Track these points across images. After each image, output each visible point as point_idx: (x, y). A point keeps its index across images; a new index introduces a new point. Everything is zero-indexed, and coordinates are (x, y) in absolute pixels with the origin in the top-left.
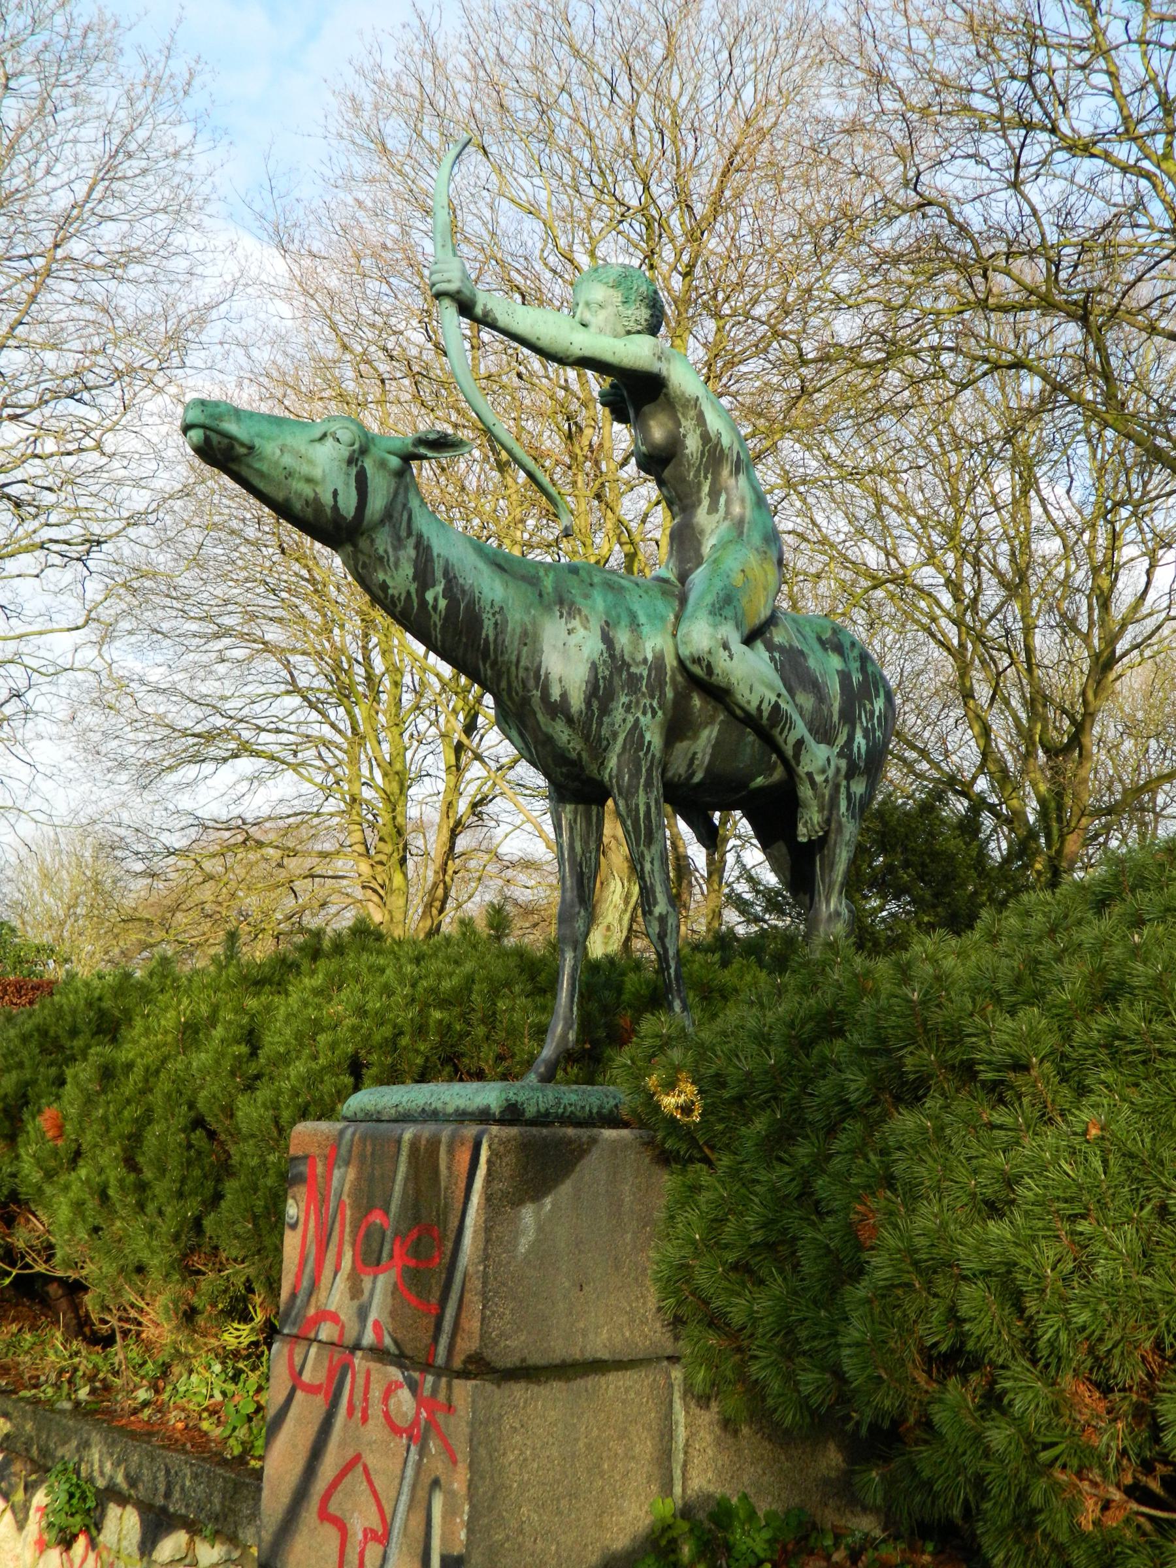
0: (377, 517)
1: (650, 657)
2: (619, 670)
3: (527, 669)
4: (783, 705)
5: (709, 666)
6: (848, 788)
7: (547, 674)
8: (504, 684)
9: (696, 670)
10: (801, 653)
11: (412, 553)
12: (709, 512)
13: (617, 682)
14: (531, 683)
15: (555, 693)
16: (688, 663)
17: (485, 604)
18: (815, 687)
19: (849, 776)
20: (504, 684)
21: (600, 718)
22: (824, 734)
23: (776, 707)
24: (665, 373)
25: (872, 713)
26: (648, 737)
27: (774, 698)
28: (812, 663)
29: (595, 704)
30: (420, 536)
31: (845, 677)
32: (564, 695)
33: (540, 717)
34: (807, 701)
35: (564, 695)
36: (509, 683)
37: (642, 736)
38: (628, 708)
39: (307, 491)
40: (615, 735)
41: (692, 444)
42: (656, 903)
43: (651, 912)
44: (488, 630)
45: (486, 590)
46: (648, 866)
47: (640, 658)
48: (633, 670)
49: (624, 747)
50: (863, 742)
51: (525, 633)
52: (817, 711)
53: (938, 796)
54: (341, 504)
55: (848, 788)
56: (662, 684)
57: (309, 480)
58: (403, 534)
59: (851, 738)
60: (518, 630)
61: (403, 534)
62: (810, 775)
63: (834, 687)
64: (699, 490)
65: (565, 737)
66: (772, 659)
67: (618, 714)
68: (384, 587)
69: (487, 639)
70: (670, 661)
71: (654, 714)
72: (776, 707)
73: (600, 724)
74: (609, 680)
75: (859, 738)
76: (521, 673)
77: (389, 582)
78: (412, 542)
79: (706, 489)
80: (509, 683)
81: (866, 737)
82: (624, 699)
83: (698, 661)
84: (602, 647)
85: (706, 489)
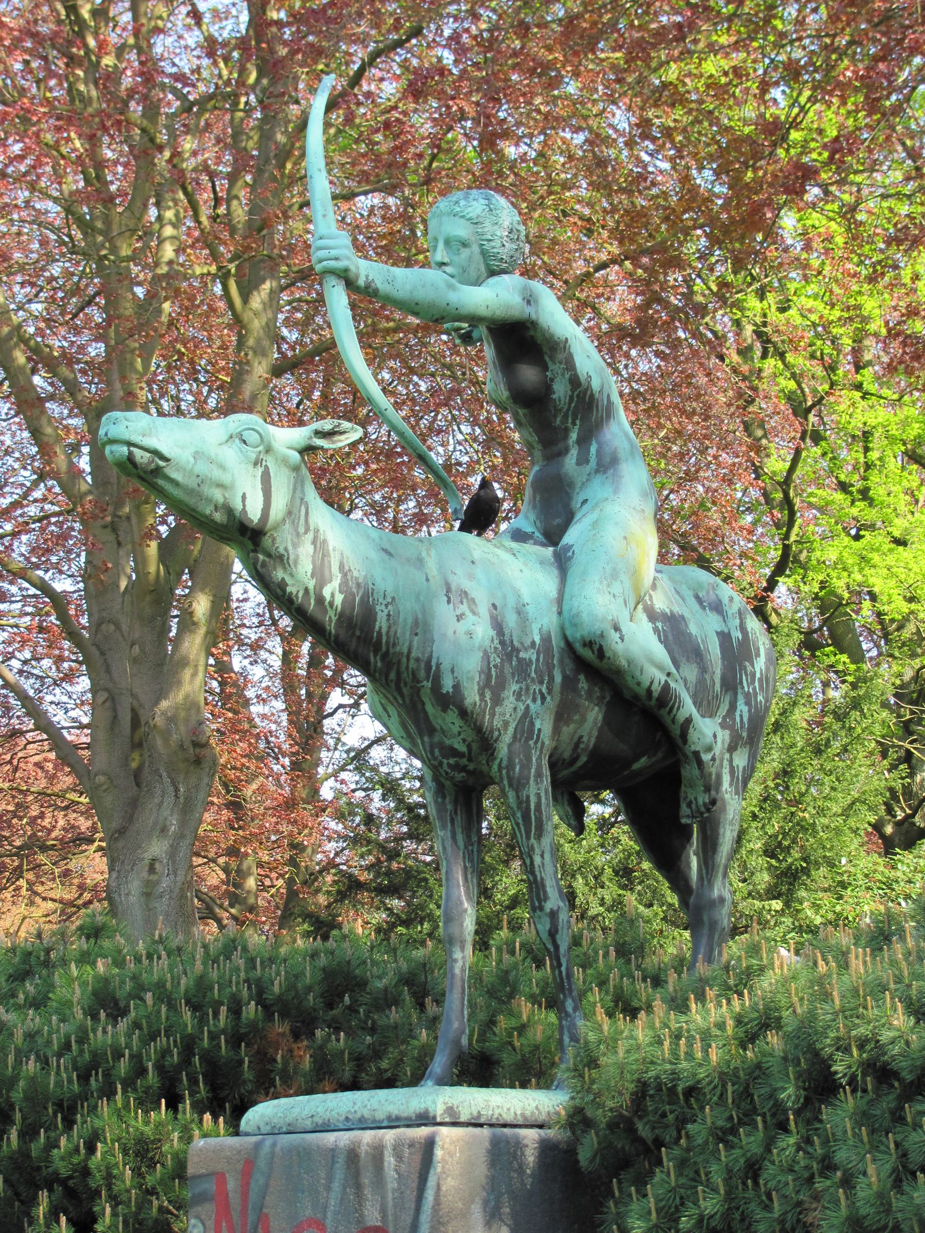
0: (280, 516)
1: (537, 639)
2: (509, 656)
3: (418, 660)
4: (673, 685)
5: (601, 649)
6: (731, 761)
7: (438, 665)
8: (393, 676)
9: (587, 654)
10: (682, 617)
11: (311, 549)
12: (579, 463)
13: (507, 670)
14: (422, 674)
15: (447, 685)
16: (578, 647)
17: (379, 596)
18: (696, 654)
19: (731, 749)
20: (393, 676)
21: (493, 709)
22: (707, 706)
23: (666, 686)
24: (534, 317)
25: (753, 675)
26: (538, 725)
27: (663, 678)
28: (693, 629)
29: (488, 695)
30: (317, 531)
31: (724, 637)
32: (457, 687)
33: (429, 708)
34: (691, 672)
35: (457, 687)
36: (399, 674)
37: (532, 724)
38: (518, 696)
39: (218, 496)
40: (506, 724)
41: (560, 390)
42: (546, 898)
43: (541, 908)
44: (381, 622)
45: (379, 582)
46: (537, 860)
47: (528, 643)
48: (522, 655)
49: (515, 737)
50: (745, 709)
51: (416, 623)
52: (701, 682)
53: (882, 836)
54: (248, 508)
55: (731, 761)
56: (550, 668)
57: (220, 485)
58: (302, 530)
59: (733, 707)
60: (410, 621)
61: (302, 530)
62: (697, 754)
63: (714, 650)
64: (566, 437)
65: (765, 984)
66: (656, 630)
67: (509, 701)
68: (283, 585)
69: (379, 633)
70: (557, 643)
71: (543, 698)
72: (666, 686)
73: (493, 715)
74: (500, 668)
75: (742, 707)
76: (412, 664)
77: (288, 580)
78: (310, 535)
79: (574, 436)
80: (399, 674)
81: (748, 703)
82: (515, 687)
83: (589, 644)
84: (492, 633)
85: (574, 436)
